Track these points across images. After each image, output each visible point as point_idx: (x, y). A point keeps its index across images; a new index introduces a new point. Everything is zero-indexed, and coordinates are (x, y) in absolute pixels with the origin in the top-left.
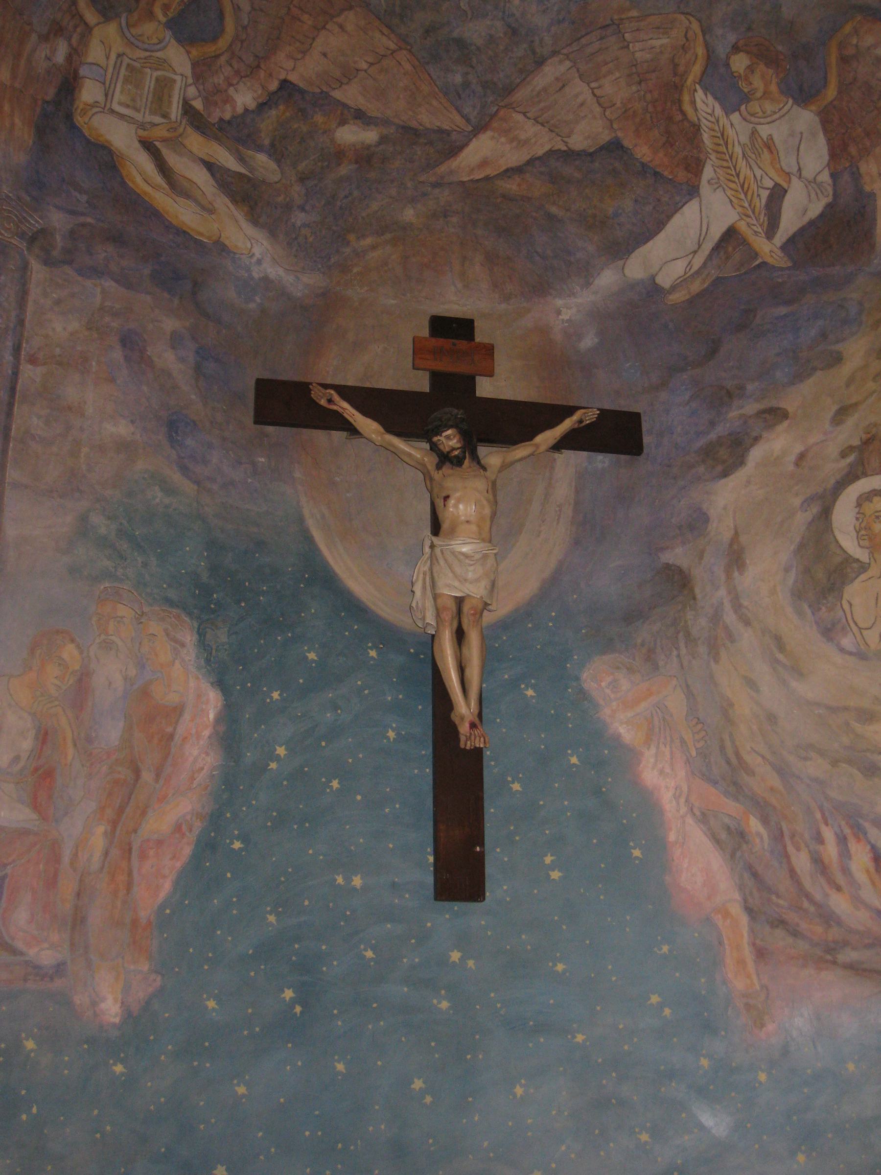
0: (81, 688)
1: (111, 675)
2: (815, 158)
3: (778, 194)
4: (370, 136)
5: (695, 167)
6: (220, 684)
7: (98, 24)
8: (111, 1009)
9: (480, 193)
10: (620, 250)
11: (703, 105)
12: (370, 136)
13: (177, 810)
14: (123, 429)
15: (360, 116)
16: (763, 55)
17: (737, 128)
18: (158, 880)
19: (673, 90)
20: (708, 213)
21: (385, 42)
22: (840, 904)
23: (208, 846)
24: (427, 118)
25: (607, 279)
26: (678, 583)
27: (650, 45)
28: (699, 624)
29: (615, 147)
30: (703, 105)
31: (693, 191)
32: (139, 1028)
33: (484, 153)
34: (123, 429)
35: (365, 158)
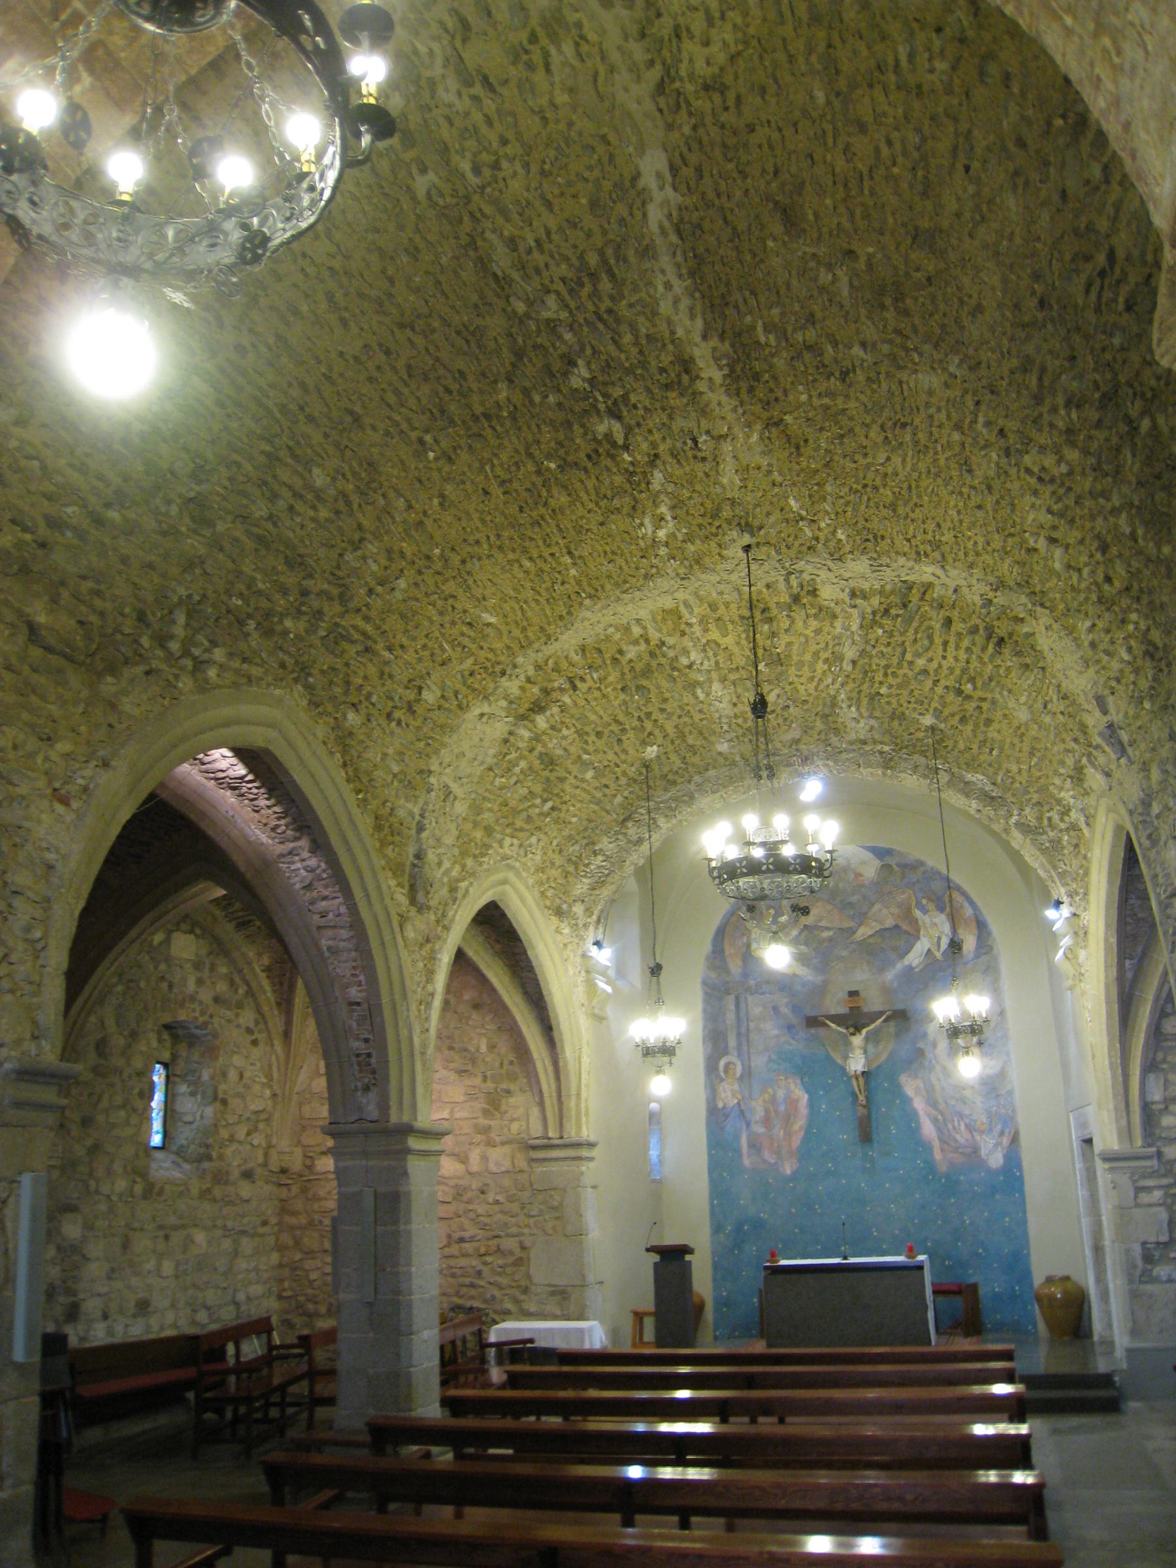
0: (774, 1100)
1: (781, 1094)
2: (947, 928)
3: (939, 939)
4: (831, 933)
5: (918, 931)
6: (807, 1092)
7: (783, 842)
8: (788, 1172)
9: (862, 943)
10: (902, 956)
11: (918, 913)
12: (831, 933)
13: (800, 1124)
14: (776, 1032)
15: (828, 929)
16: (930, 900)
17: (927, 919)
18: (796, 1141)
19: (909, 910)
20: (921, 946)
21: (830, 907)
22: (958, 1137)
23: (808, 1132)
24: (845, 925)
25: (899, 966)
26: (920, 1053)
27: (901, 897)
28: (927, 1064)
29: (897, 927)
30: (918, 913)
31: (918, 938)
32: (794, 1177)
33: (863, 932)
34: (776, 1032)
35: (830, 939)
